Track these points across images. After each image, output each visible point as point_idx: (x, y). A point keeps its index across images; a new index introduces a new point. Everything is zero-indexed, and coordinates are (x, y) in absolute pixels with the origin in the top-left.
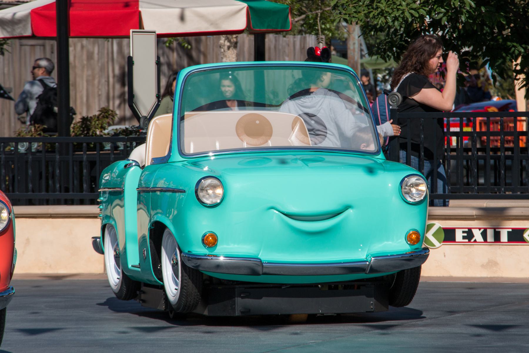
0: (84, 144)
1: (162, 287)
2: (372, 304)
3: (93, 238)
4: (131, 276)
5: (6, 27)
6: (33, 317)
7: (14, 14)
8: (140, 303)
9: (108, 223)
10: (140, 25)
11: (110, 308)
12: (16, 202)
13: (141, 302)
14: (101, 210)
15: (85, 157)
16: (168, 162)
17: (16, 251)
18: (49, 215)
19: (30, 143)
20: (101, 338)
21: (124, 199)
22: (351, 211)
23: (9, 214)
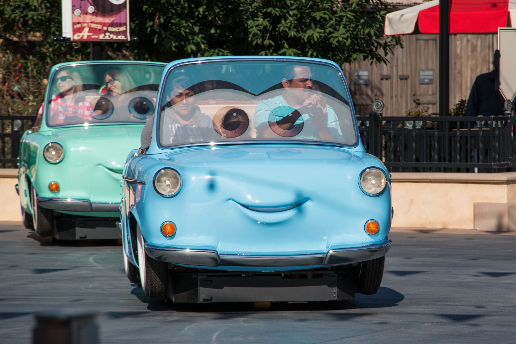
0: (458, 123)
2: (335, 292)
15: (458, 133)
18: (429, 181)
19: (414, 121)
20: (466, 280)
22: (310, 204)
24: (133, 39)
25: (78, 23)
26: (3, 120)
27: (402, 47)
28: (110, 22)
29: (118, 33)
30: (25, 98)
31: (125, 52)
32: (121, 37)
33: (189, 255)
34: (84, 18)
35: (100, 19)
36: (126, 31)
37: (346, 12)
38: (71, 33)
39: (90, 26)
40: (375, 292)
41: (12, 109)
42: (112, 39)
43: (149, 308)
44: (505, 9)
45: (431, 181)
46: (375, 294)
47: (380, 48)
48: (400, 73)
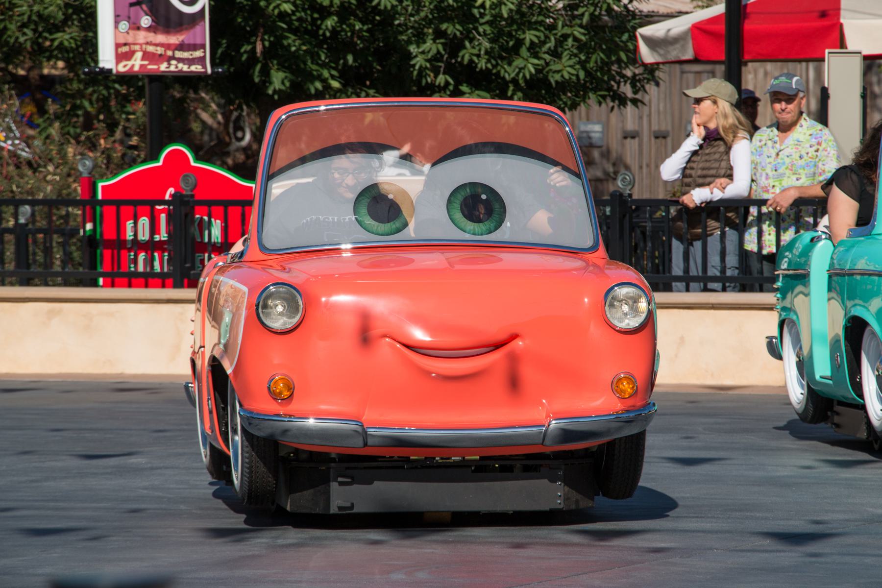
1: (863, 407)
3: (767, 338)
4: (819, 391)
5: (658, 49)
6: (685, 443)
7: (669, 30)
8: (832, 427)
9: (788, 317)
10: (841, 43)
11: (791, 433)
12: (656, 288)
13: (834, 426)
14: (778, 300)
16: (872, 233)
17: (658, 353)
18: (711, 306)
20: (778, 474)
21: (809, 284)
23: (649, 304)
24: (216, 70)
25: (125, 44)
26: (209, 206)
27: (657, 84)
28: (177, 42)
29: (190, 62)
30: (41, 169)
31: (203, 95)
32: (196, 68)
33: (314, 428)
34: (135, 36)
35: (161, 38)
36: (204, 57)
37: (571, 27)
38: (114, 61)
39: (144, 49)
40: (630, 495)
41: (17, 187)
42: (181, 71)
43: (246, 522)
44: (836, 18)
45: (715, 306)
46: (631, 497)
47: (625, 85)
48: (655, 127)
